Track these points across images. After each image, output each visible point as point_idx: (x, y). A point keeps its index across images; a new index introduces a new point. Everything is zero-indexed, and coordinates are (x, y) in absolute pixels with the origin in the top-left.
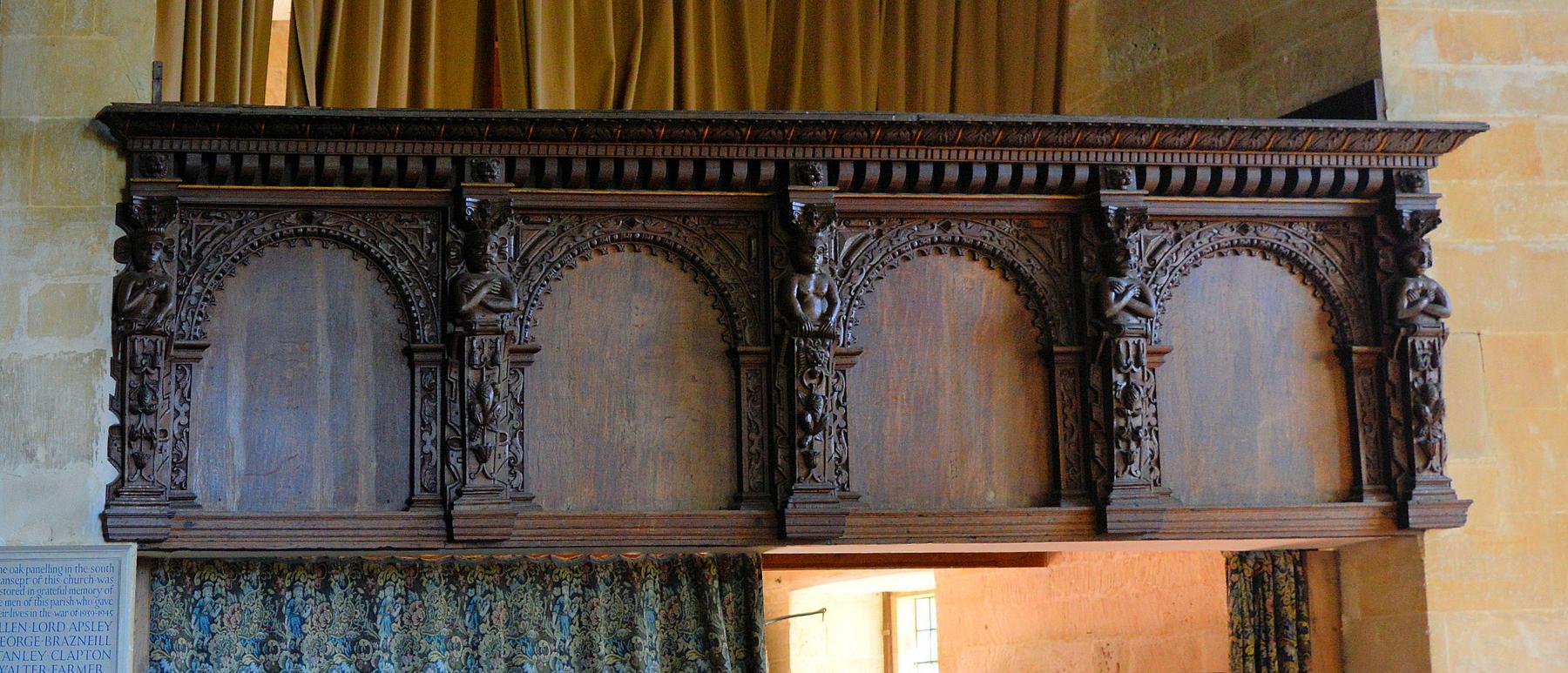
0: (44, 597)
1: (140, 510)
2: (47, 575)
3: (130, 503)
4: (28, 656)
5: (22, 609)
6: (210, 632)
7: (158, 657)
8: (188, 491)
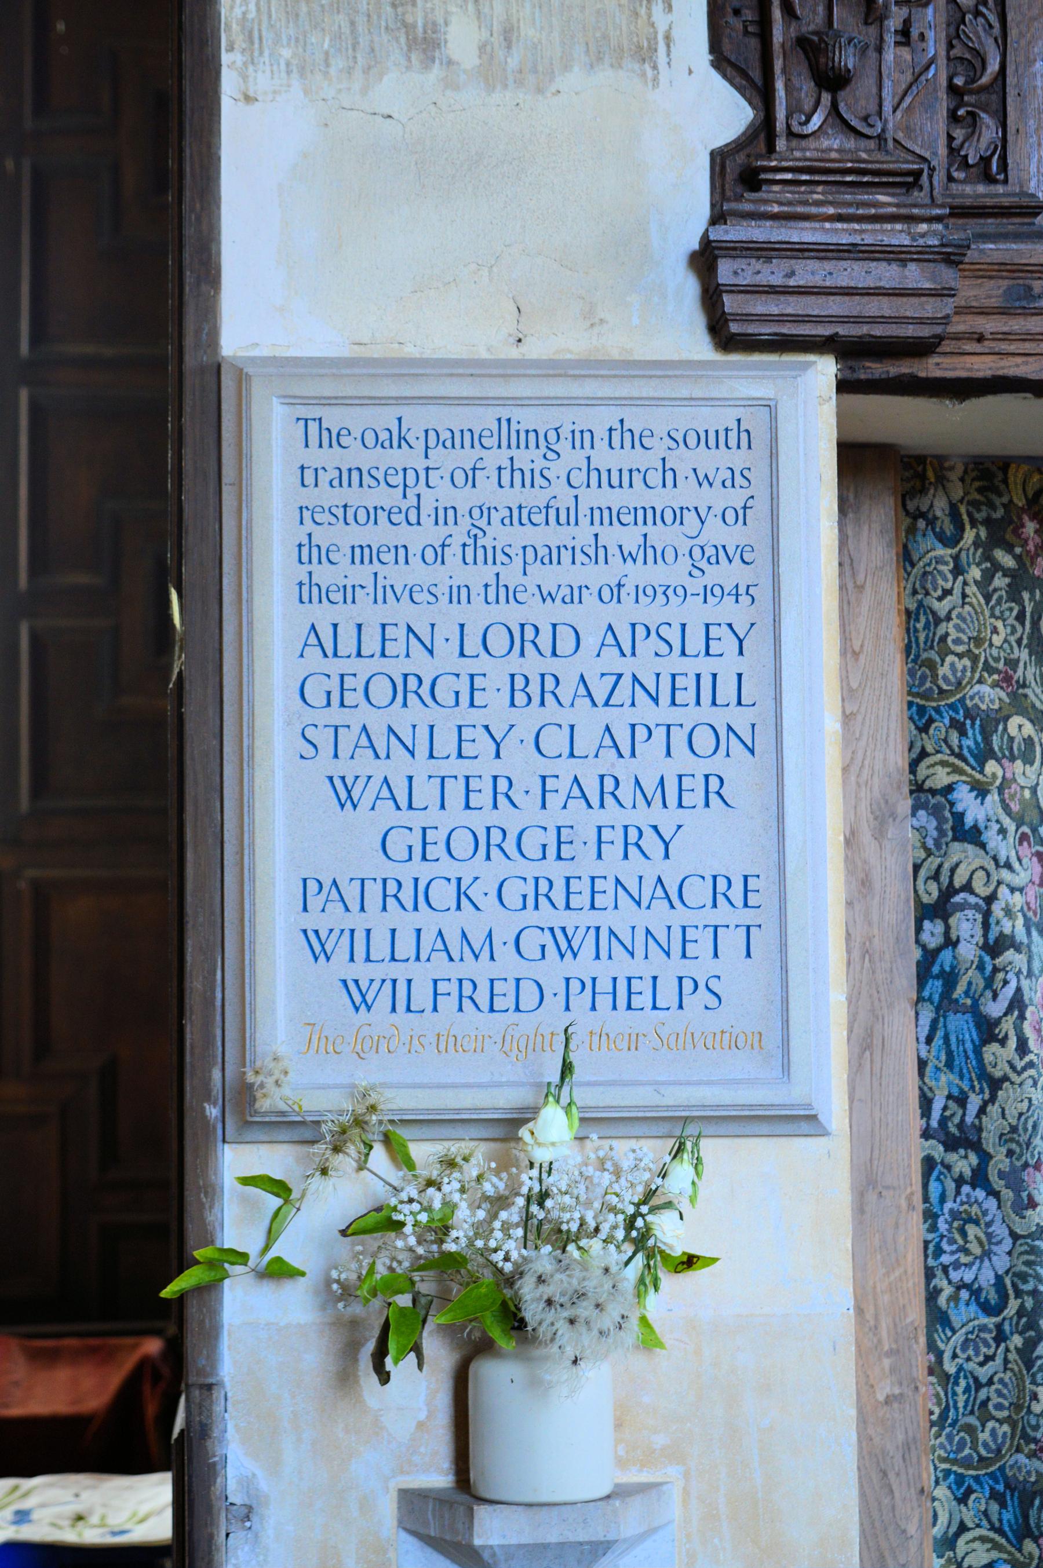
0: (498, 534)
1: (842, 234)
2: (502, 458)
3: (800, 209)
4: (446, 743)
5: (417, 573)
6: (984, 1075)
7: (942, 778)
8: (1013, 187)
